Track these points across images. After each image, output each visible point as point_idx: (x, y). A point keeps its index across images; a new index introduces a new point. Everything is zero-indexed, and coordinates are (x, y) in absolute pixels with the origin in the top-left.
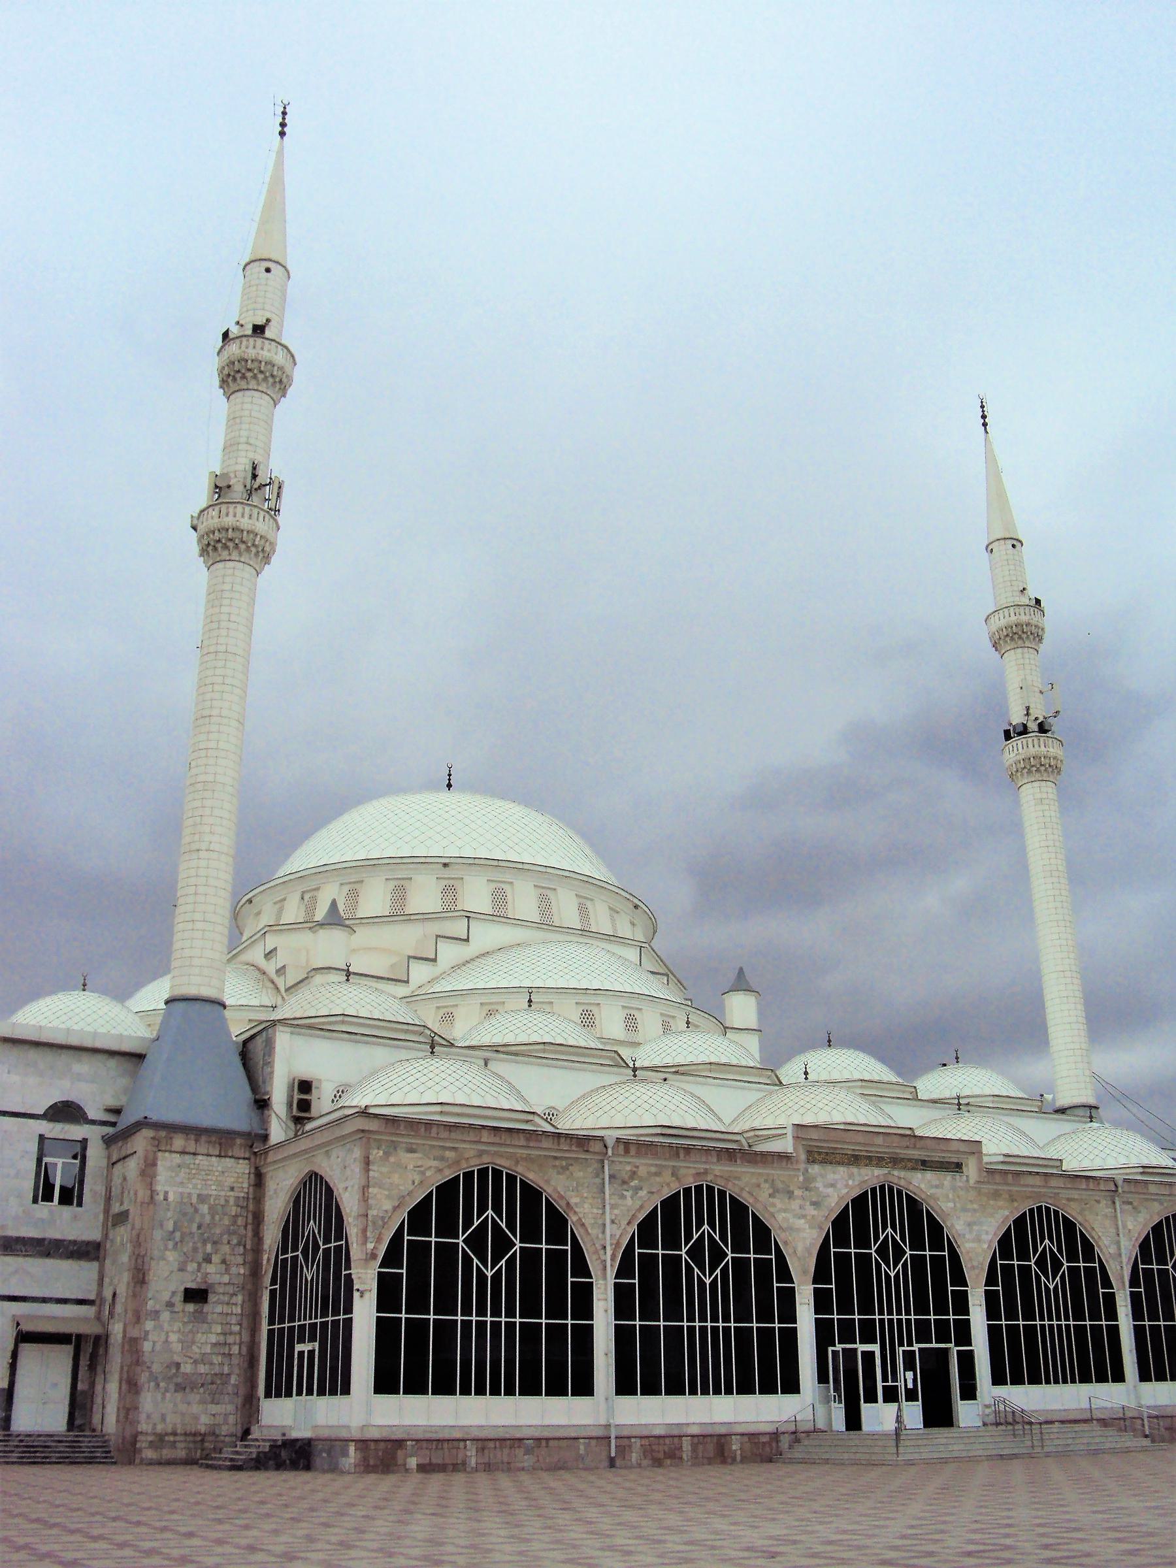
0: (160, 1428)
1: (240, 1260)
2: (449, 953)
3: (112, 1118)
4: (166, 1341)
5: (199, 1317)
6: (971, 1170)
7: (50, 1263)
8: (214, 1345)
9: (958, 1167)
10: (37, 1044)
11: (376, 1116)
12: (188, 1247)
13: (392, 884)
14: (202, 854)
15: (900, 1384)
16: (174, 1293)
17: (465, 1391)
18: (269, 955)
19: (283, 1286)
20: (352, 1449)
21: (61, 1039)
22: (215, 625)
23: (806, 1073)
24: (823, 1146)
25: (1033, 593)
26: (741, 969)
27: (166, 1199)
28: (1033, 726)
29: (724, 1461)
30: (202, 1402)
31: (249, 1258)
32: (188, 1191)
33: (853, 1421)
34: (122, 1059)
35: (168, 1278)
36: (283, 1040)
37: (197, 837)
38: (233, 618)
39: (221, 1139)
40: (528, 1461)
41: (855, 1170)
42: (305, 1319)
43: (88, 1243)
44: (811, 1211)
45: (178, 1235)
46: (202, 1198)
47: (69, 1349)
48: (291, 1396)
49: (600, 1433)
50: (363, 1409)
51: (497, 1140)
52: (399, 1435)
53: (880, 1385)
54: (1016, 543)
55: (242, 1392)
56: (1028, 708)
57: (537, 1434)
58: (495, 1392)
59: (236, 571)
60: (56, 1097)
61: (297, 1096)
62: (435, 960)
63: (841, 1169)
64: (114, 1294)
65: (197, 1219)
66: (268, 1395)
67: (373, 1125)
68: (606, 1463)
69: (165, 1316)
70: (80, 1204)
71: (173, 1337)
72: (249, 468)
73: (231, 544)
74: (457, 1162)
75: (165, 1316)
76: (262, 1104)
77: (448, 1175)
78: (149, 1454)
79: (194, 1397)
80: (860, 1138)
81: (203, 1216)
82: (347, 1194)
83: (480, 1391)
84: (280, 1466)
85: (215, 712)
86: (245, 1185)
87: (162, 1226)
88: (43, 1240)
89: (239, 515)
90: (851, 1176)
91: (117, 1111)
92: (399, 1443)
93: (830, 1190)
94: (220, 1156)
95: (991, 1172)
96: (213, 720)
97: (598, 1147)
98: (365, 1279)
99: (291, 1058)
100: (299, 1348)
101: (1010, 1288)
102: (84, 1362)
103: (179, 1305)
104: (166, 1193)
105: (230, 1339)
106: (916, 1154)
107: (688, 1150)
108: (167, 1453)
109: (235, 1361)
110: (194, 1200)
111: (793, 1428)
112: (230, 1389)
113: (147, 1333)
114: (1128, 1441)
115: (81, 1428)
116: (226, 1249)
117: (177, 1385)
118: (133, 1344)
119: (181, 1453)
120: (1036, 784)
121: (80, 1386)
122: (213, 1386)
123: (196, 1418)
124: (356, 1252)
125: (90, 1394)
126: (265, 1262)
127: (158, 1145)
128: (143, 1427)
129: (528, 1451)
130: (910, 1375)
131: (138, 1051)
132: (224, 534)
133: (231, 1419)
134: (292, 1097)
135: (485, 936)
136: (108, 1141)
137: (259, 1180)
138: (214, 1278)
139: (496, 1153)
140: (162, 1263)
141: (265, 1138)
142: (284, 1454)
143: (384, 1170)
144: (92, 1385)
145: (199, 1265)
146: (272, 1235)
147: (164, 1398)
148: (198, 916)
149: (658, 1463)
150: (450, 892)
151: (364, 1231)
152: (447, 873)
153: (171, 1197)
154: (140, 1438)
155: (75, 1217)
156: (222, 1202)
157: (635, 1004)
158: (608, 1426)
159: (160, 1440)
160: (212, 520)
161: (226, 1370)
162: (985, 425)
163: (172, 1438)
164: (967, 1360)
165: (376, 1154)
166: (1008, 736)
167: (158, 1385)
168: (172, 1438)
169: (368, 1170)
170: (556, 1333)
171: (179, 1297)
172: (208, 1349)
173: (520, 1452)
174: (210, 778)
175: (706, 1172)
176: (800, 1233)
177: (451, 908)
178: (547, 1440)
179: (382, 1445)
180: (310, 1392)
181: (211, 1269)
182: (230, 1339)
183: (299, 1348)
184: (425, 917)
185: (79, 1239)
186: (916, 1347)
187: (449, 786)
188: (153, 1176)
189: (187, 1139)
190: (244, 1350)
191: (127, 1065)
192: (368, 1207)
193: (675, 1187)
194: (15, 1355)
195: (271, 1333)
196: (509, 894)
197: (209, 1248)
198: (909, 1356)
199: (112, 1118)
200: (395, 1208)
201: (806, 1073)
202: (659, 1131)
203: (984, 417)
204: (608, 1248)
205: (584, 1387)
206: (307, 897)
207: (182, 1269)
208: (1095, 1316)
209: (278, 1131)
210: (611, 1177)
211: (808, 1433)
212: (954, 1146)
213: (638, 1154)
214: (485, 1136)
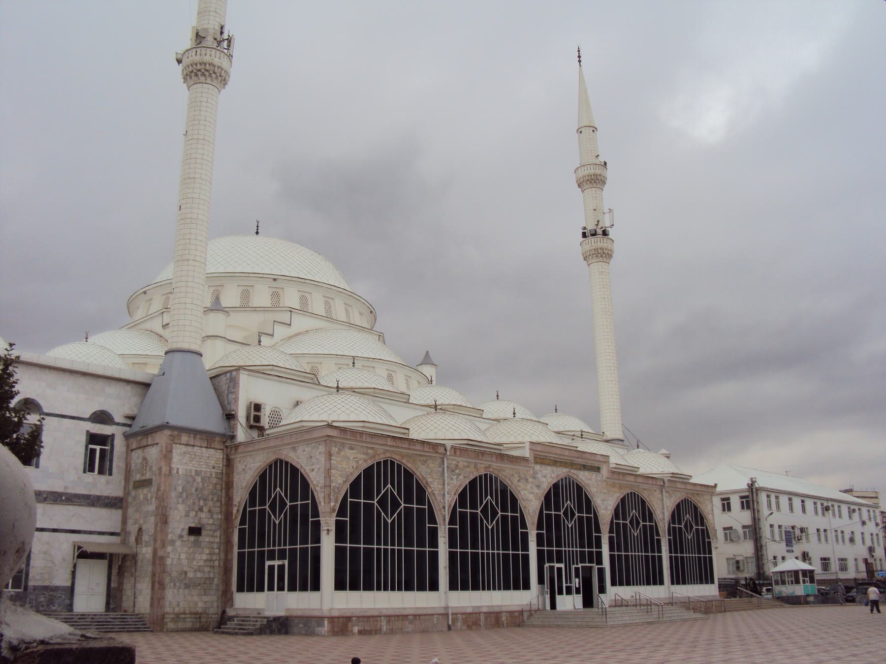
0: (177, 610)
1: (218, 510)
2: (280, 332)
3: (129, 422)
4: (179, 559)
5: (197, 544)
6: (604, 471)
7: (93, 510)
8: (205, 561)
9: (598, 469)
10: (84, 374)
11: (336, 427)
12: (190, 502)
13: (212, 289)
14: (191, 262)
15: (573, 585)
16: (183, 530)
17: (379, 589)
18: (165, 326)
19: (252, 528)
20: (326, 622)
21: (100, 372)
22: (197, 122)
23: (514, 414)
24: (543, 455)
25: (602, 159)
26: (427, 353)
28: (600, 231)
29: (499, 627)
30: (199, 595)
31: (223, 510)
32: (189, 468)
33: (553, 606)
34: (134, 386)
35: (179, 522)
36: (244, 379)
38: (208, 119)
39: (207, 437)
40: (410, 628)
41: (555, 468)
42: (274, 545)
43: (116, 498)
44: (536, 490)
45: (184, 494)
46: (198, 473)
47: (104, 563)
48: (263, 590)
49: (442, 611)
50: (330, 599)
51: (394, 444)
52: (348, 614)
53: (564, 585)
54: (594, 130)
55: (221, 588)
57: (413, 612)
58: (393, 589)
59: (206, 89)
60: (96, 407)
61: (253, 413)
62: (272, 335)
63: (549, 468)
64: (140, 530)
65: (195, 485)
66: (240, 589)
67: (334, 433)
68: (446, 629)
69: (178, 543)
70: (110, 474)
71: (183, 556)
72: (218, 28)
73: (207, 73)
74: (374, 456)
75: (178, 543)
76: (230, 417)
77: (370, 463)
78: (171, 625)
79: (195, 592)
80: (558, 451)
81: (198, 483)
82: (314, 473)
83: (386, 589)
84: (272, 633)
85: (197, 176)
87: (175, 489)
88: (90, 496)
89: (213, 55)
90: (553, 472)
91: (133, 418)
92: (349, 618)
93: (544, 479)
95: (613, 473)
97: (441, 450)
98: (328, 523)
99: (249, 391)
100: (268, 563)
101: (465, 528)
102: (115, 571)
103: (186, 538)
104: (178, 469)
105: (214, 557)
106: (580, 461)
107: (483, 453)
108: (181, 625)
109: (216, 570)
110: (193, 474)
111: (528, 608)
112: (214, 587)
113: (169, 553)
114: (692, 615)
115: (114, 610)
116: (210, 503)
117: (185, 584)
118: (158, 560)
119: (189, 625)
121: (113, 585)
122: (204, 585)
123: (196, 603)
124: (322, 507)
125: (120, 589)
126: (235, 512)
127: (174, 440)
128: (168, 609)
129: (411, 622)
130: (577, 580)
131: (147, 381)
132: (203, 66)
133: (215, 605)
135: (300, 323)
136: (127, 437)
137: (229, 463)
138: (205, 521)
139: (393, 452)
140: (176, 512)
141: (233, 437)
142: (274, 625)
143: (339, 459)
144: (121, 584)
145: (197, 512)
146: (240, 496)
147: (178, 592)
149: (469, 627)
150: (275, 295)
151: (329, 495)
152: (274, 284)
153: (180, 473)
154: (167, 616)
155: (108, 483)
156: (208, 475)
157: (393, 368)
158: (447, 608)
159: (177, 617)
160: (194, 58)
161: (212, 575)
162: (580, 61)
163: (183, 616)
164: (601, 572)
165: (335, 450)
166: (584, 235)
167: (175, 585)
168: (183, 616)
169: (330, 460)
170: (421, 554)
171: (186, 532)
172: (202, 563)
173: (407, 623)
175: (489, 467)
176: (531, 502)
177: (276, 307)
178: (419, 615)
179: (341, 620)
180: (281, 588)
181: (203, 515)
182: (214, 557)
183: (268, 563)
184: (264, 309)
185: (111, 495)
186: (580, 565)
187: (257, 233)
188: (171, 459)
190: (222, 563)
191: (138, 390)
192: (331, 481)
193: (476, 474)
194: (75, 566)
195: (241, 555)
196: (309, 299)
197: (202, 503)
198: (577, 569)
199: (129, 422)
200: (345, 482)
201: (514, 414)
202: (466, 442)
203: (579, 57)
204: (447, 508)
205: (434, 587)
207: (187, 516)
208: (421, 544)
209: (241, 435)
210: (448, 467)
211: (535, 611)
212: (599, 458)
213: (460, 456)
214: (390, 442)
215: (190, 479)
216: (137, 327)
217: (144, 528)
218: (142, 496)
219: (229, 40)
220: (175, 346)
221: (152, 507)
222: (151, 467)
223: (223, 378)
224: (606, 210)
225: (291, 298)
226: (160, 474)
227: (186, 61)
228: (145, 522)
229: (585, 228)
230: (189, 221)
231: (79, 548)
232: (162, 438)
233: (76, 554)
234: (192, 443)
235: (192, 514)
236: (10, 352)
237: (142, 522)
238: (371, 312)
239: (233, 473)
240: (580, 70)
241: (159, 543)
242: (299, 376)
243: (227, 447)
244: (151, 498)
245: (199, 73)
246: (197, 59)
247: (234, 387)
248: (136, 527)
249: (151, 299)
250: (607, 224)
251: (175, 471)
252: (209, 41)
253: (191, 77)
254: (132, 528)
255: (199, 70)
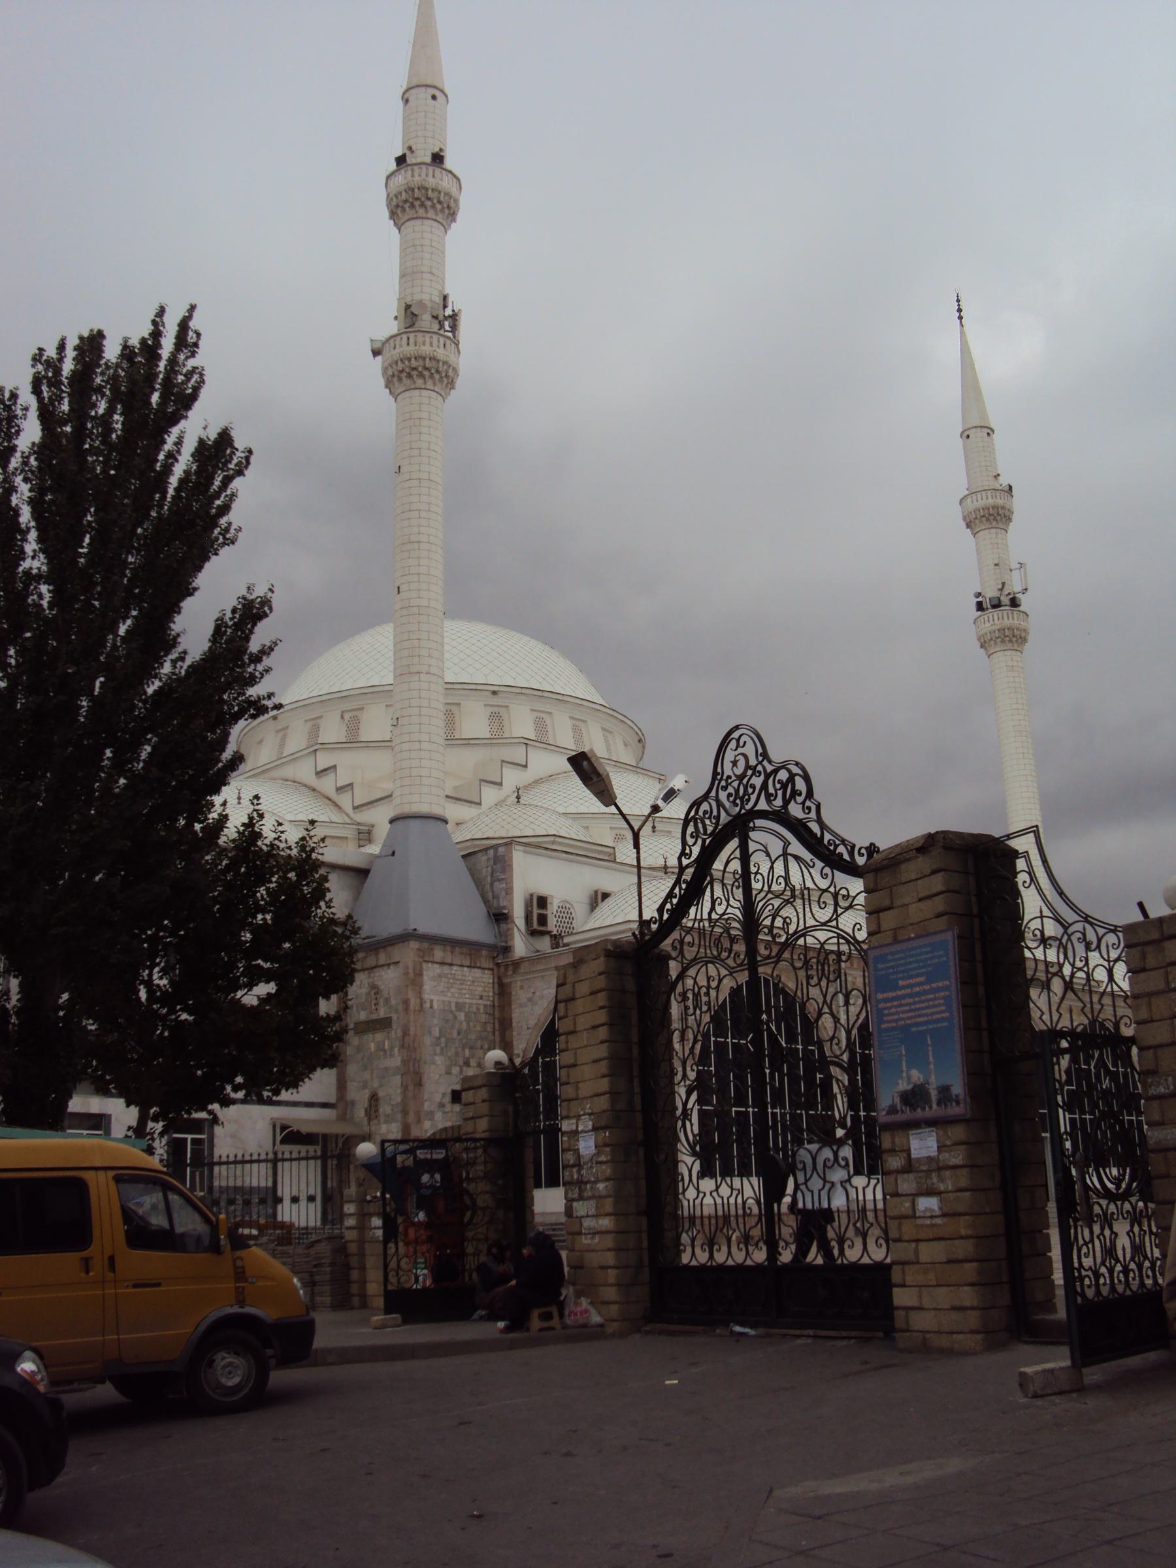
2: (512, 778)
12: (451, 1053)
14: (424, 677)
16: (444, 1095)
25: (1004, 481)
27: (431, 1007)
28: (1005, 600)
32: (447, 999)
36: (519, 859)
37: (416, 660)
38: (433, 447)
45: (443, 1040)
46: (460, 1007)
56: (1003, 584)
61: (536, 911)
62: (500, 784)
65: (457, 1026)
72: (438, 300)
73: (426, 373)
76: (500, 917)
81: (461, 1023)
85: (423, 538)
86: (491, 994)
94: (469, 967)
96: (422, 546)
99: (530, 875)
103: (448, 1107)
104: (432, 1001)
110: (453, 1008)
120: (1009, 653)
121: (329, 1185)
127: (425, 957)
132: (421, 362)
134: (531, 912)
137: (503, 991)
140: (433, 1067)
141: (507, 950)
145: (461, 1067)
148: (425, 737)
150: (496, 718)
152: (496, 700)
153: (436, 1006)
162: (960, 318)
166: (980, 607)
171: (448, 1099)
174: (424, 603)
188: (421, 986)
189: (444, 951)
196: (548, 722)
197: (467, 1051)
203: (960, 310)
206: (347, 716)
207: (448, 1073)
209: (520, 946)
215: (450, 1017)
216: (266, 775)
217: (381, 1094)
218: (372, 1045)
219: (454, 317)
220: (407, 809)
221: (396, 1061)
222: (387, 1000)
223: (482, 859)
224: (1014, 565)
225: (522, 723)
226: (407, 1009)
227: (391, 354)
228: (381, 1086)
229: (979, 595)
230: (415, 610)
231: (283, 1128)
232: (408, 953)
233: (279, 1138)
234: (448, 960)
235: (456, 1070)
236: (312, 833)
237: (376, 1084)
238: (640, 741)
239: (510, 1004)
240: (962, 333)
241: (411, 1118)
242: (583, 848)
243: (498, 965)
244: (392, 1048)
245: (415, 373)
246: (411, 350)
247: (504, 871)
248: (366, 1094)
249: (287, 727)
250: (1017, 588)
251: (428, 1005)
252: (425, 321)
253: (400, 379)
254: (359, 1096)
255: (415, 369)
